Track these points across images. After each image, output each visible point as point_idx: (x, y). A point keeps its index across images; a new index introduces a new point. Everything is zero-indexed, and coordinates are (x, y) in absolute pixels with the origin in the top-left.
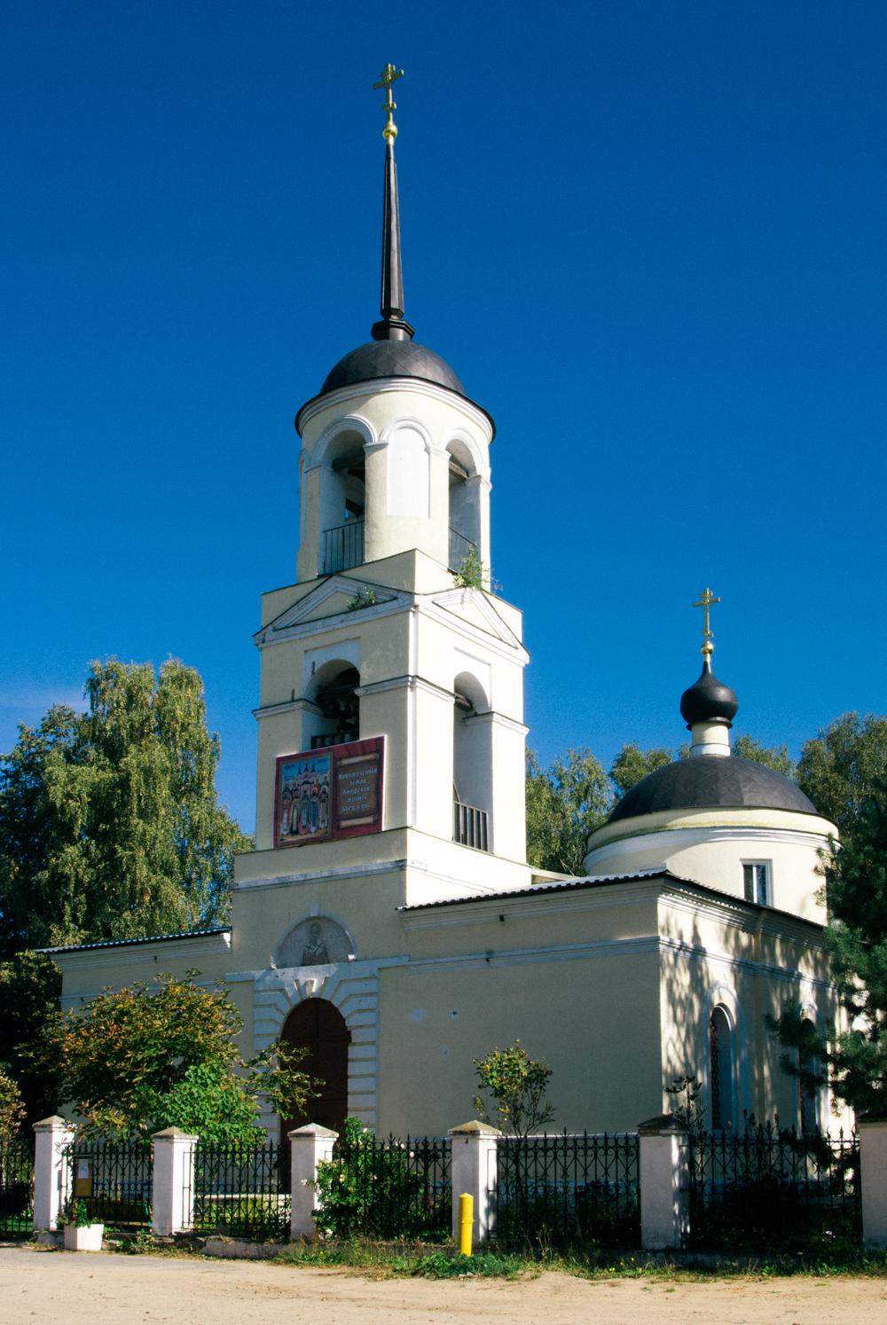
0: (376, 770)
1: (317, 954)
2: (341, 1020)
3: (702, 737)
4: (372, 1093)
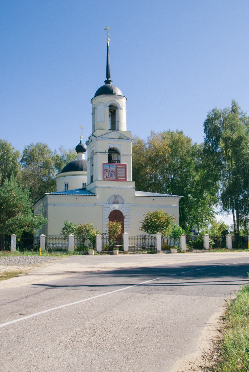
2: (113, 212)
3: (82, 155)
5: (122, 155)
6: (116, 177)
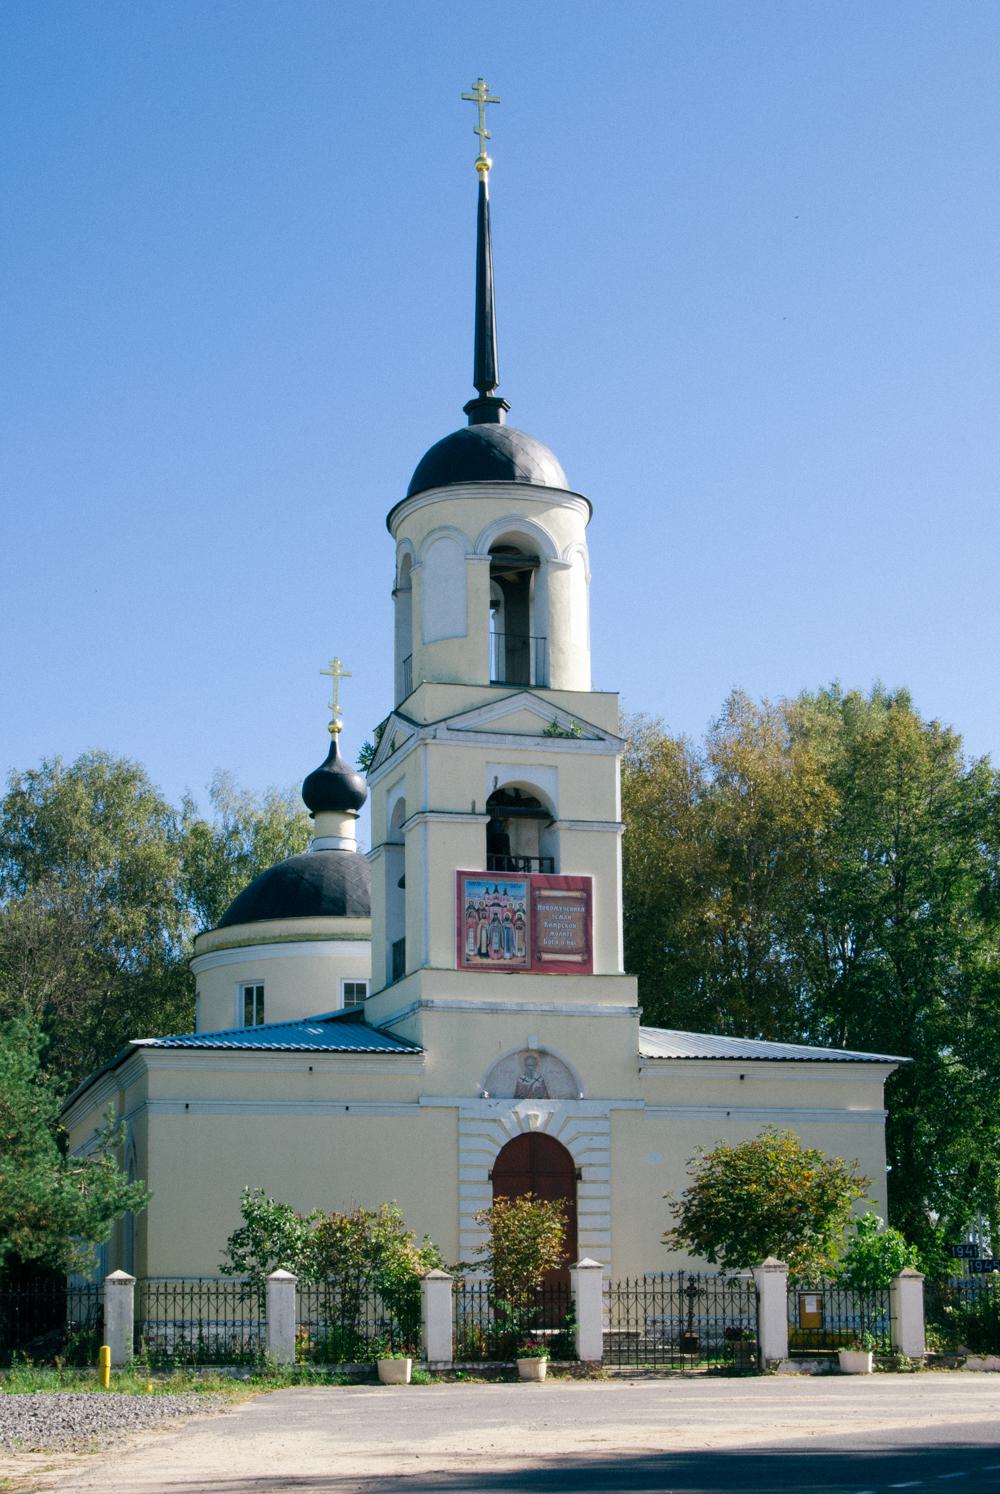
0: (583, 909)
1: (534, 1086)
4: (606, 1230)
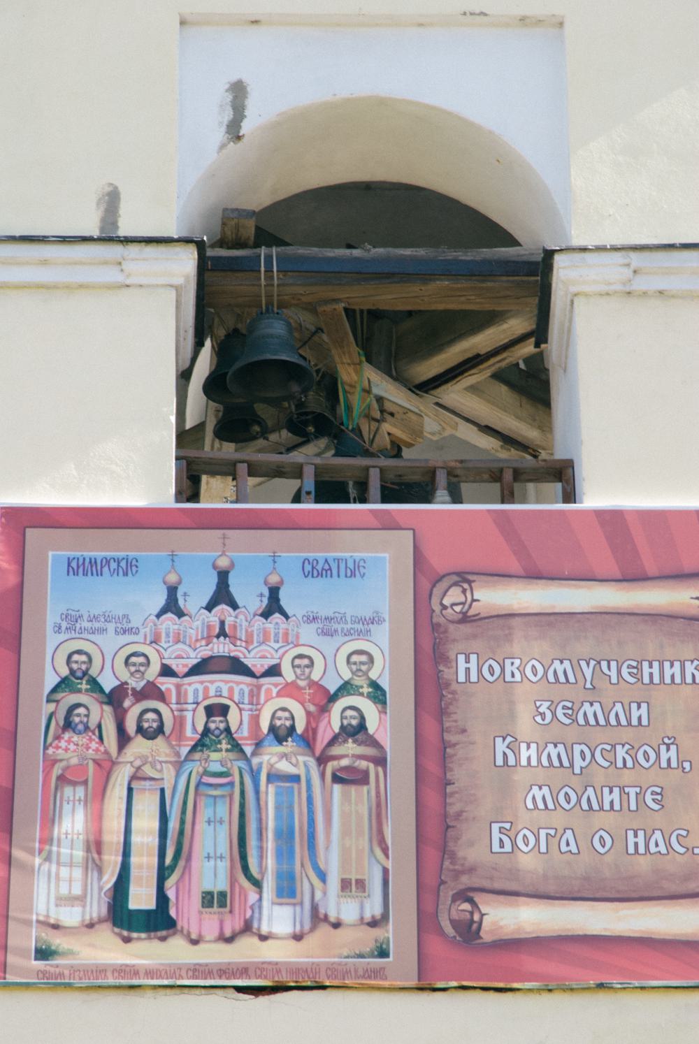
5: (610, 270)
6: (427, 892)
